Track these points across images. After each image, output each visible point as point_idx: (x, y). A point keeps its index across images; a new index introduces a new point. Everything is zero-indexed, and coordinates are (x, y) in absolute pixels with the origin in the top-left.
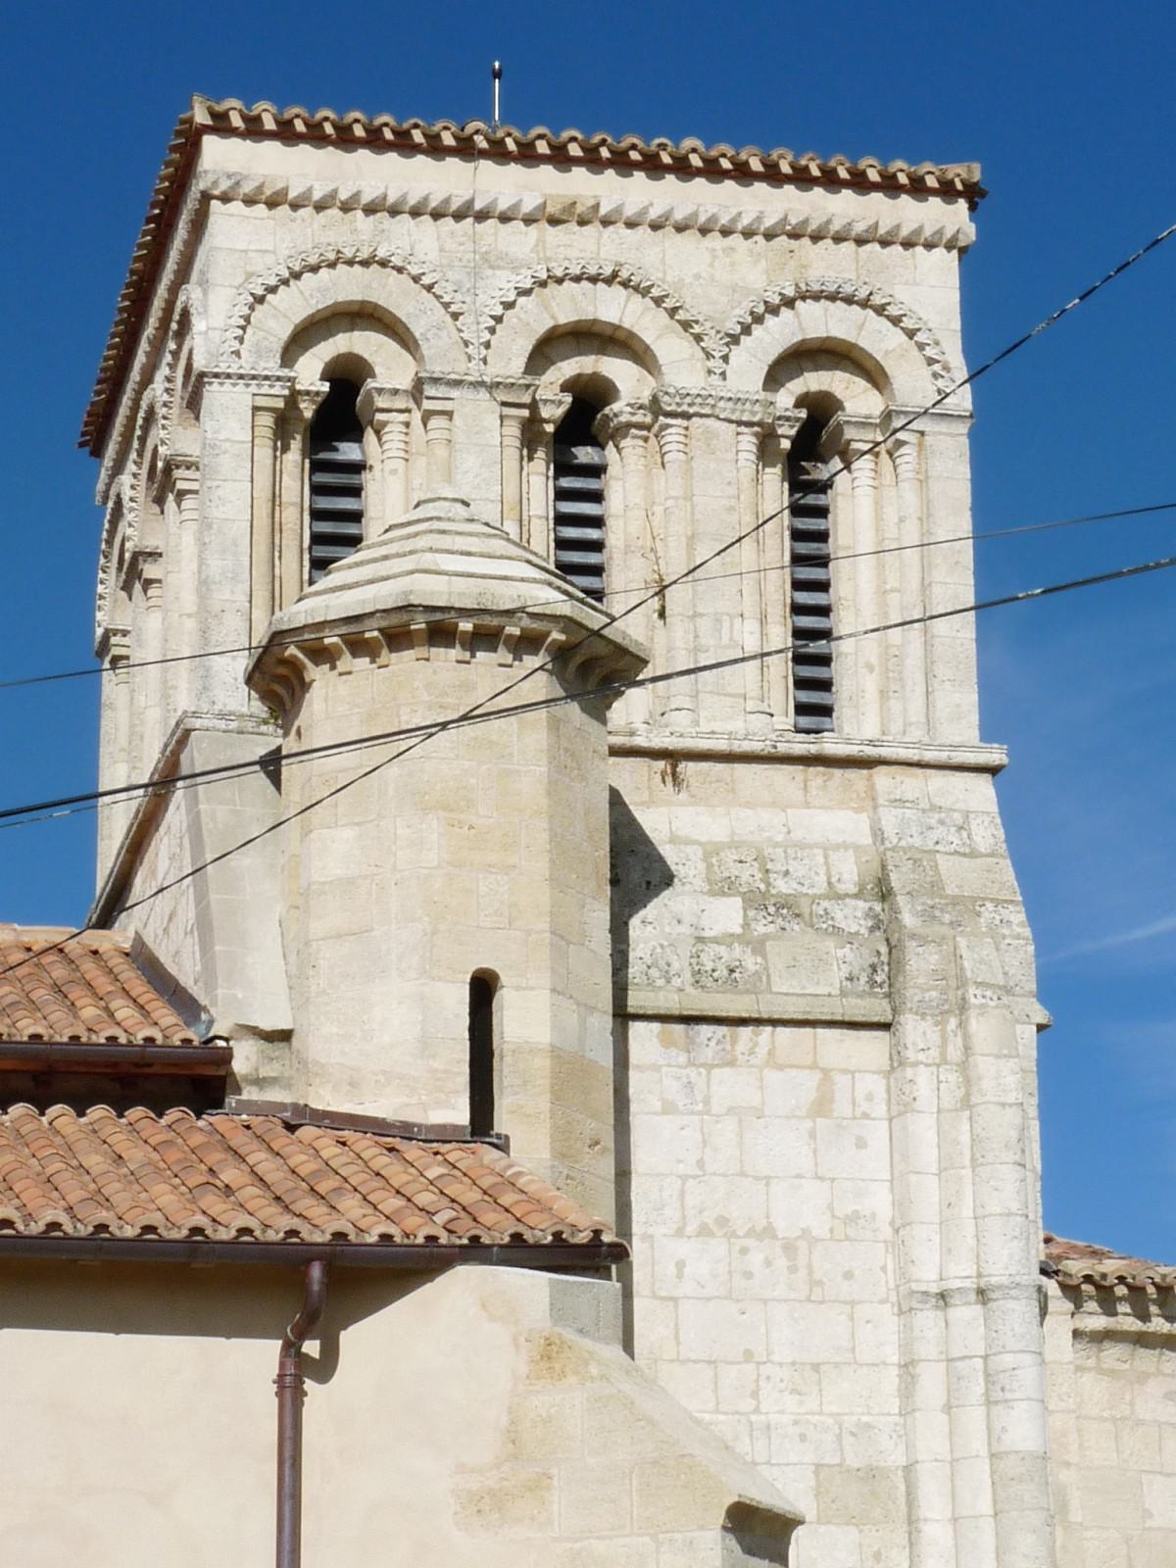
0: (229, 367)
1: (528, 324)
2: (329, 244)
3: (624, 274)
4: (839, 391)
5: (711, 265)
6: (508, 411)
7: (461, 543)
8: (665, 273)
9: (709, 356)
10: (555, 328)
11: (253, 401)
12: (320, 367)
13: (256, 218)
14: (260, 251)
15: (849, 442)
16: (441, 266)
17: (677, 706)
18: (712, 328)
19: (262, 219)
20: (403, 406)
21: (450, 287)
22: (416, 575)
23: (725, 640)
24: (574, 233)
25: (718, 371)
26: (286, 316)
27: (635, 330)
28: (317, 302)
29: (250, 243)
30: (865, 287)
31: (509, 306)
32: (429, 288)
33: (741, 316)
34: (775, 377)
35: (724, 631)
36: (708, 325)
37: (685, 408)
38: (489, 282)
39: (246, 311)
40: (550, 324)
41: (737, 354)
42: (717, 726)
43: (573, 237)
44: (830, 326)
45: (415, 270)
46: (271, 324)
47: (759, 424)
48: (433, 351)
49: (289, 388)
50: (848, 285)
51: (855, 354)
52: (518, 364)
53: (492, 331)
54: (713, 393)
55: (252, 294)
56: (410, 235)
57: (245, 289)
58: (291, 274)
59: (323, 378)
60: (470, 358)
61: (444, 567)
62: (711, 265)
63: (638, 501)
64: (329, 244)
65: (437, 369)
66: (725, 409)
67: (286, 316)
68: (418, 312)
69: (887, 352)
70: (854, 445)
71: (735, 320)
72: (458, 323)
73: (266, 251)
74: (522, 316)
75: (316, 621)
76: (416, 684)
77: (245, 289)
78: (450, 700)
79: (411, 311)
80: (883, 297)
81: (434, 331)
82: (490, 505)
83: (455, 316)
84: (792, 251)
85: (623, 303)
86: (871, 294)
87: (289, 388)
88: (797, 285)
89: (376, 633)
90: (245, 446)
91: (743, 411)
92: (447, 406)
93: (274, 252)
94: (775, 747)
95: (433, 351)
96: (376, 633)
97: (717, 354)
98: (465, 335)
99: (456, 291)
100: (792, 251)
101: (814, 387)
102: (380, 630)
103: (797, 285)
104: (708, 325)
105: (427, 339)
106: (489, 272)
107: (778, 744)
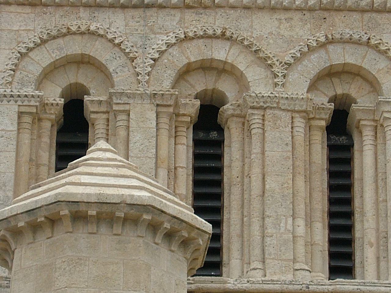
0: (5, 91)
1: (174, 62)
2: (63, 25)
3: (228, 34)
4: (353, 93)
5: (279, 27)
6: (161, 109)
7: (99, 170)
8: (252, 33)
9: (276, 76)
10: (189, 64)
11: (18, 109)
12: (59, 90)
13: (24, 13)
14: (26, 30)
15: (359, 121)
16: (126, 34)
17: (253, 267)
18: (277, 60)
19: (28, 14)
20: (105, 110)
21: (129, 45)
22: (67, 186)
23: (282, 230)
24: (201, 14)
25: (280, 83)
26: (38, 64)
27: (235, 63)
28: (56, 56)
29: (20, 26)
30: (366, 35)
31: (162, 53)
32: (119, 45)
33: (294, 54)
34: (313, 87)
35: (282, 225)
36: (275, 59)
37: (262, 104)
38: (153, 40)
39: (16, 61)
40: (186, 61)
41: (293, 76)
42: (275, 278)
43: (201, 16)
44: (347, 57)
45: (110, 36)
46: (31, 68)
47: (304, 111)
48: (118, 79)
49: (38, 101)
50: (356, 34)
51: (362, 73)
52: (167, 84)
53: (152, 66)
54: (277, 95)
55: (19, 52)
56: (109, 19)
57: (16, 50)
58: (41, 41)
59: (62, 96)
60: (139, 82)
61: (238, 232)
62: (279, 27)
63: (238, 157)
64: (63, 25)
65: (119, 88)
66: (284, 104)
67: (38, 64)
68: (112, 59)
69: (379, 70)
70: (362, 123)
71: (290, 56)
72: (134, 64)
73: (29, 30)
74: (170, 58)
75: (13, 214)
76: (65, 246)
77: (16, 50)
78: (84, 255)
79: (108, 58)
80: (377, 40)
81: (121, 68)
82: (148, 160)
83: (132, 60)
84: (325, 18)
85: (228, 49)
86: (369, 39)
87: (38, 101)
88: (326, 36)
89: (43, 219)
90: (13, 133)
91: (295, 104)
92: (127, 107)
93: (34, 30)
94: (308, 288)
95: (118, 79)
96: (43, 219)
97: (280, 75)
98: (137, 70)
99: (132, 46)
100: (325, 18)
101: (339, 91)
102: (46, 217)
103: (326, 36)
104: (275, 59)
105: (117, 73)
106: (153, 36)
107: (310, 286)
